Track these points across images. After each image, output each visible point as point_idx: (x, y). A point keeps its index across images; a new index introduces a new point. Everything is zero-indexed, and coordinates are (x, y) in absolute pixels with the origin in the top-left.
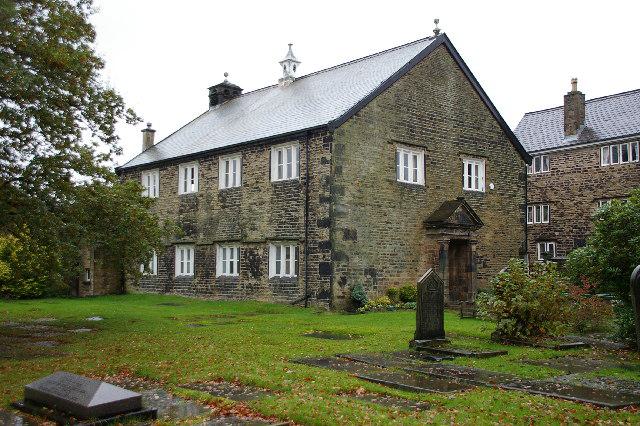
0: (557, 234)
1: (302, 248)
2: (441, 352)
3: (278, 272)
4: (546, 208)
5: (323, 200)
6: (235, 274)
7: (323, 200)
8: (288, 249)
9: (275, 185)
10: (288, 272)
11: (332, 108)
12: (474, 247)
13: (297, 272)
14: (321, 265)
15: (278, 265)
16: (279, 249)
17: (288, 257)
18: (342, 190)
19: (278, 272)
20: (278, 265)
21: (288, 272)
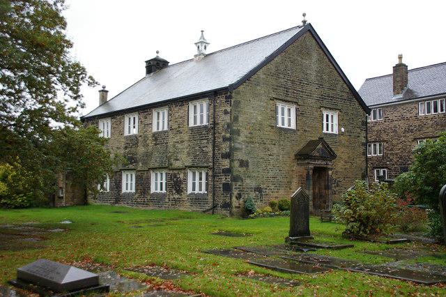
0: (388, 163)
1: (210, 173)
3: (194, 189)
4: (380, 145)
5: (225, 139)
7: (225, 139)
8: (201, 174)
10: (200, 190)
12: (330, 172)
13: (207, 190)
16: (194, 174)
17: (201, 179)
21: (200, 190)
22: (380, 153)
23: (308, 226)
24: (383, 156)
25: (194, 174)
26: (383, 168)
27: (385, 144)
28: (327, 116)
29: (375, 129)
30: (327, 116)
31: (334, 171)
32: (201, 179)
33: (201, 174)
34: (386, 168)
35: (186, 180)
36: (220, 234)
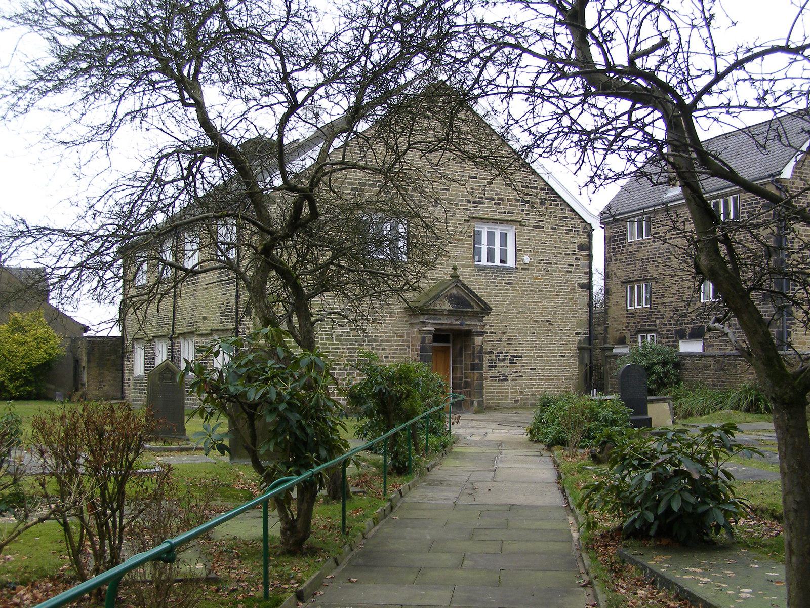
0: (658, 322)
12: (478, 340)
24: (651, 308)
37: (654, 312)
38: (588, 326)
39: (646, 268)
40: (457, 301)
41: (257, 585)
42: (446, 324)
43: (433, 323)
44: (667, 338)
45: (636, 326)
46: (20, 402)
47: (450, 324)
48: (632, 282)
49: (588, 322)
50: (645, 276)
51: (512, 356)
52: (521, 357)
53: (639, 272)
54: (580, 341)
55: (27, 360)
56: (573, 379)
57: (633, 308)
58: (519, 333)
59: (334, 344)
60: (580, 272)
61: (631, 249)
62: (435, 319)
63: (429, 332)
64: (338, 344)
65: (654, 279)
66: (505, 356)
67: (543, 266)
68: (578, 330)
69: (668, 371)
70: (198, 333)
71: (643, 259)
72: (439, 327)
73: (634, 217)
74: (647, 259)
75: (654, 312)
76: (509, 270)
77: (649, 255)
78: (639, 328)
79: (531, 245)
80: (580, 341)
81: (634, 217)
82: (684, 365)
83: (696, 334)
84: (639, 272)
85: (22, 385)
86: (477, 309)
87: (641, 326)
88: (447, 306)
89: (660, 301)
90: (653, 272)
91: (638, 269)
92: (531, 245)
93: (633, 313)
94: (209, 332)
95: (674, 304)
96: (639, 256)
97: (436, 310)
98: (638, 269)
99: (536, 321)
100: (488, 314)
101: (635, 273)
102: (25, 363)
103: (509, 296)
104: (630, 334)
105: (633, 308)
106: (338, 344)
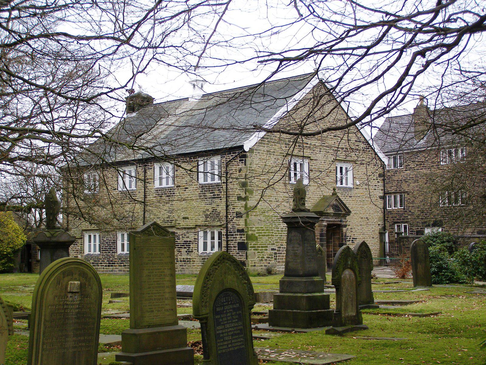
0: (409, 217)
1: (224, 232)
2: (327, 287)
3: (90, 251)
4: (401, 196)
5: (240, 198)
6: (98, 252)
7: (240, 198)
8: (123, 235)
9: (202, 186)
10: (95, 251)
11: (40, 143)
12: (344, 229)
13: (100, 251)
14: (239, 243)
15: (205, 244)
16: (205, 233)
17: (213, 238)
18: (251, 192)
19: (90, 251)
20: (205, 244)
21: (95, 251)
22: (401, 206)
23: (101, 302)
24: (404, 209)
25: (205, 233)
26: (404, 223)
27: (406, 195)
28: (341, 168)
29: (395, 178)
30: (341, 168)
31: (349, 227)
32: (213, 238)
33: (123, 235)
34: (406, 222)
35: (196, 240)
36: (398, 283)
37: (406, 211)
38: (383, 220)
39: (400, 186)
40: (335, 207)
41: (459, 322)
42: (332, 221)
43: (327, 221)
44: (416, 226)
45: (393, 219)
46: (6, 274)
47: (334, 221)
48: (391, 193)
49: (383, 218)
50: (399, 190)
51: (353, 238)
52: (356, 239)
53: (395, 188)
54: (380, 229)
55: (11, 246)
56: (377, 251)
57: (391, 208)
58: (355, 225)
59: (280, 233)
60: (379, 190)
61: (389, 174)
62: (327, 218)
63: (325, 226)
64: (281, 233)
65: (406, 192)
66: (350, 238)
67: (364, 187)
68: (379, 223)
69: (451, 245)
70: (177, 227)
71: (397, 180)
72: (329, 223)
73: (391, 155)
74: (401, 180)
75: (406, 211)
76: (350, 189)
77: (402, 178)
78: (396, 221)
79: (359, 175)
80: (380, 229)
81: (391, 155)
82: (457, 242)
83: (435, 224)
84: (395, 188)
85: (6, 263)
86: (344, 212)
87: (397, 219)
88: (331, 211)
89: (411, 205)
90: (405, 187)
91: (394, 186)
92: (359, 175)
93: (391, 212)
94: (194, 226)
95: (422, 207)
96: (395, 178)
97: (328, 213)
98: (394, 186)
99: (362, 218)
100: (349, 215)
101: (392, 188)
102: (10, 247)
103: (350, 204)
104: (389, 224)
105: (391, 208)
106: (281, 233)
